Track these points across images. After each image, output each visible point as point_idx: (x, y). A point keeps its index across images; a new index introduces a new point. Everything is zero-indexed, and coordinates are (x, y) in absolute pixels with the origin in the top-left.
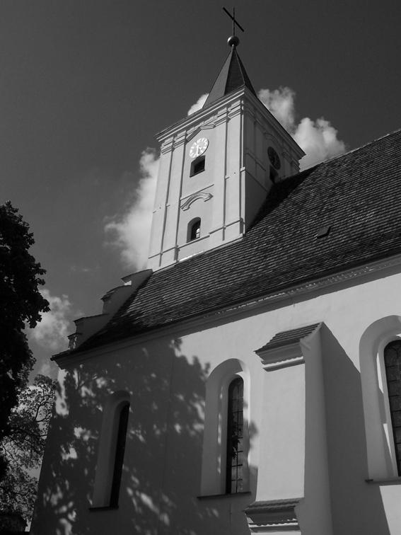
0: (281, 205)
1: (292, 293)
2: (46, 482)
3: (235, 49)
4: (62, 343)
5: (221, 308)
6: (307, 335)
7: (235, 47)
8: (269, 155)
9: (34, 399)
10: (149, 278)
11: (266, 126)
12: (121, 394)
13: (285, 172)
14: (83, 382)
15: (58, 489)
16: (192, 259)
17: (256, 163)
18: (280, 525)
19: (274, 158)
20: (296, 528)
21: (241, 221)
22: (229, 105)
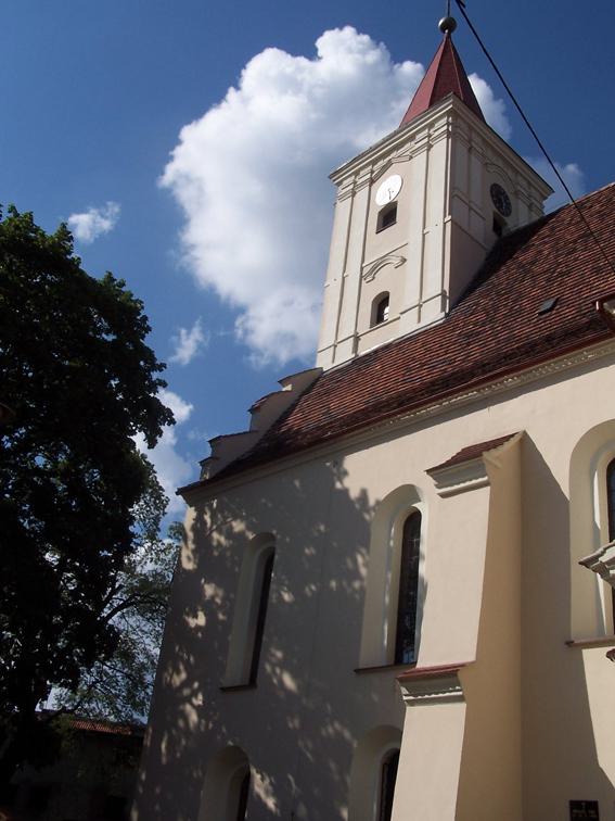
0: (504, 269)
1: (487, 392)
2: (167, 660)
3: (449, 36)
4: (190, 473)
5: (395, 414)
6: (495, 447)
7: (449, 34)
8: (492, 196)
9: (170, 556)
10: (317, 380)
11: (489, 154)
12: (265, 537)
13: (520, 218)
14: (214, 527)
15: (182, 667)
16: (376, 352)
17: (470, 209)
18: (441, 695)
19: (500, 200)
20: (460, 699)
21: (443, 294)
22: (431, 125)
